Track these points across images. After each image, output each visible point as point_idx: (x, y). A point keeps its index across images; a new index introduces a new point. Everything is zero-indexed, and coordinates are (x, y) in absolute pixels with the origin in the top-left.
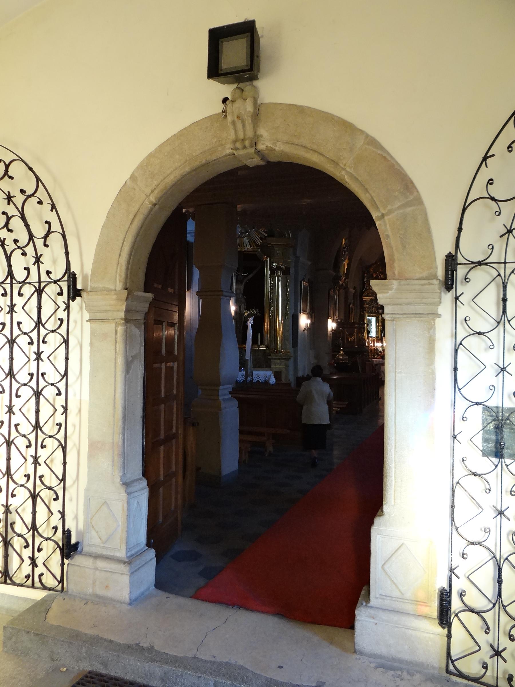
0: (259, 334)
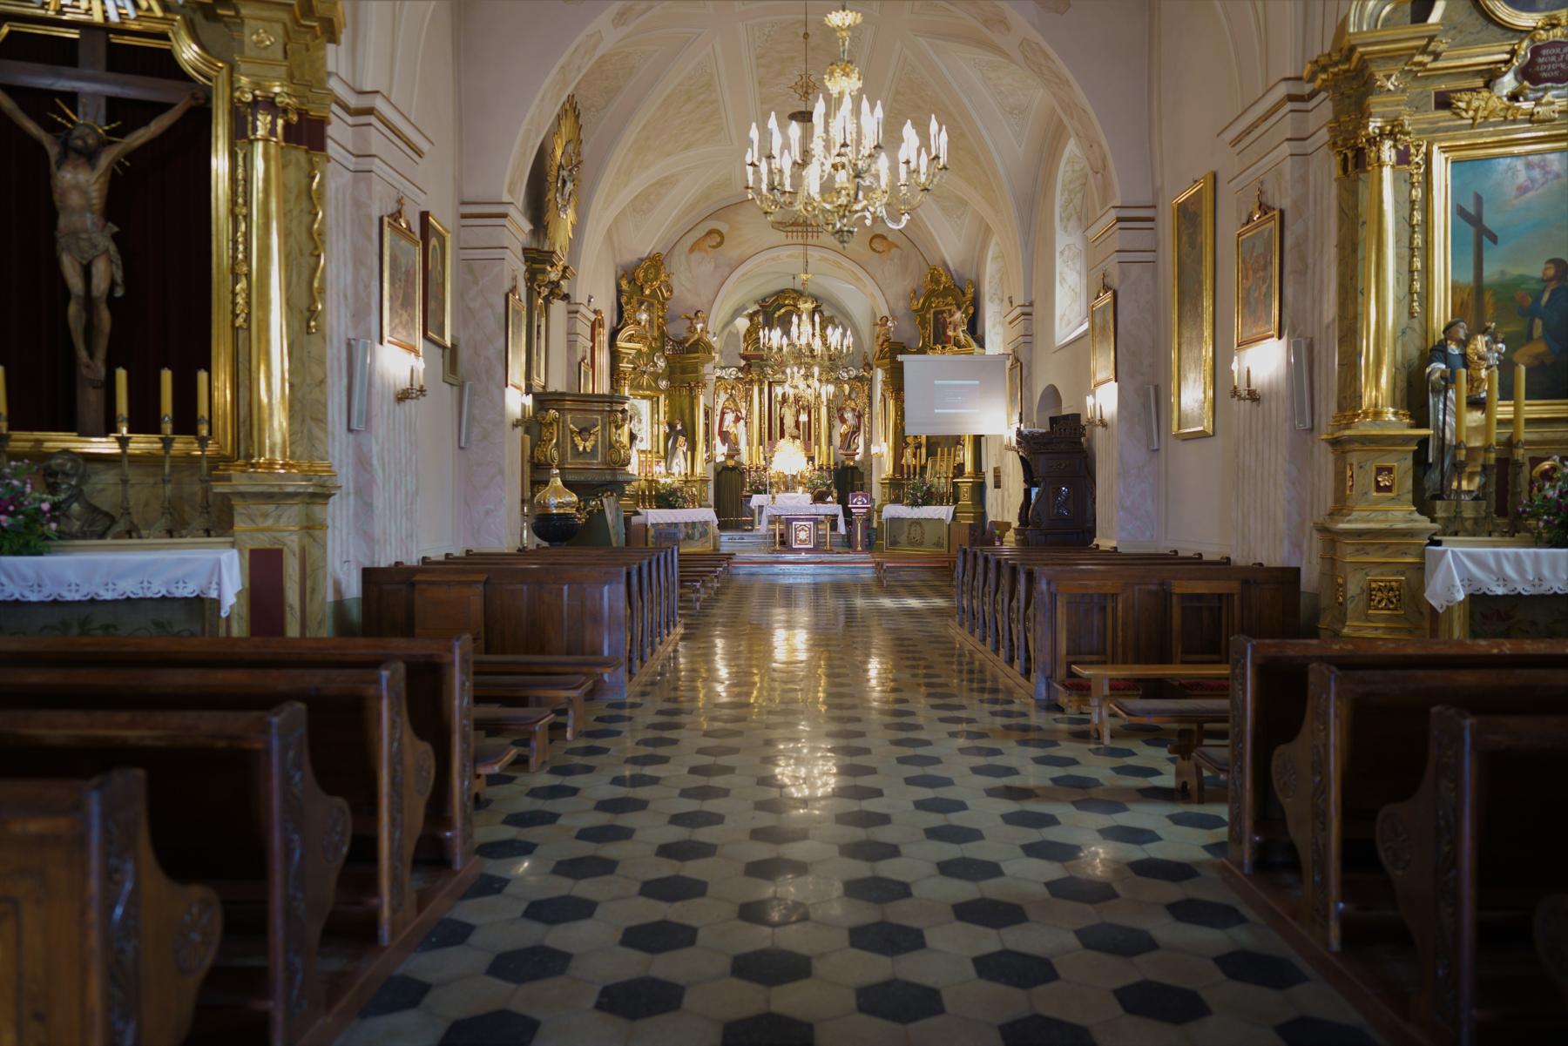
0: (167, 376)
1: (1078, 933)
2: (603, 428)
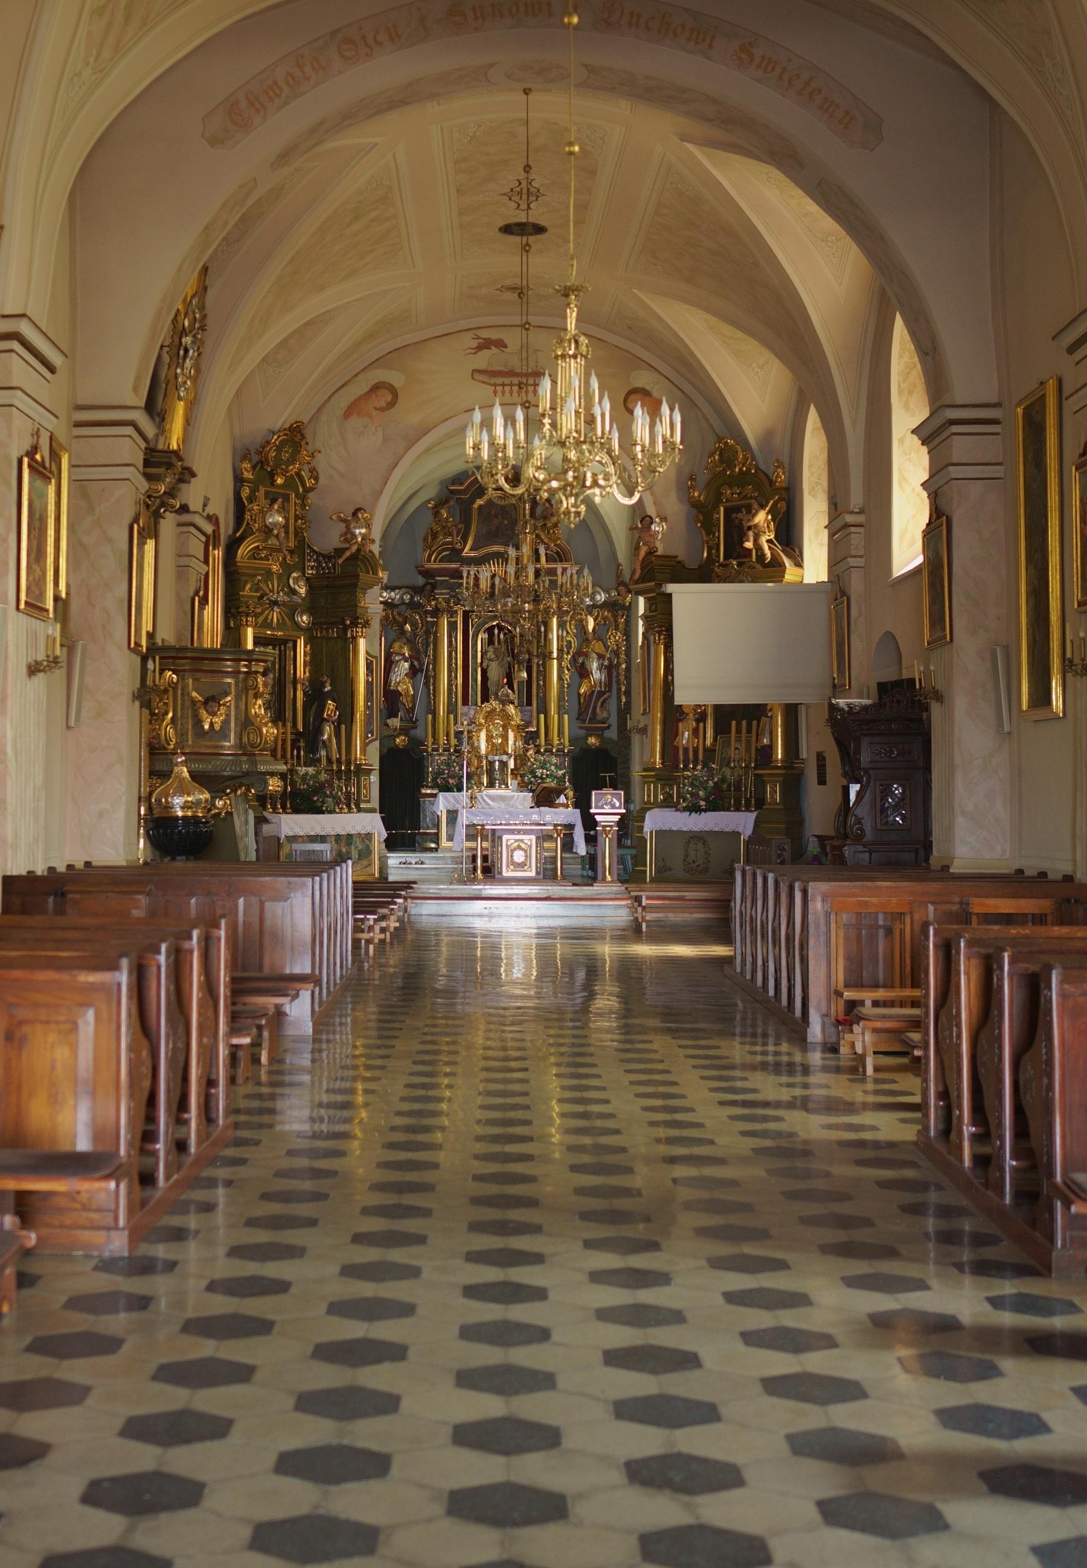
1: (766, 1170)
2: (238, 698)
